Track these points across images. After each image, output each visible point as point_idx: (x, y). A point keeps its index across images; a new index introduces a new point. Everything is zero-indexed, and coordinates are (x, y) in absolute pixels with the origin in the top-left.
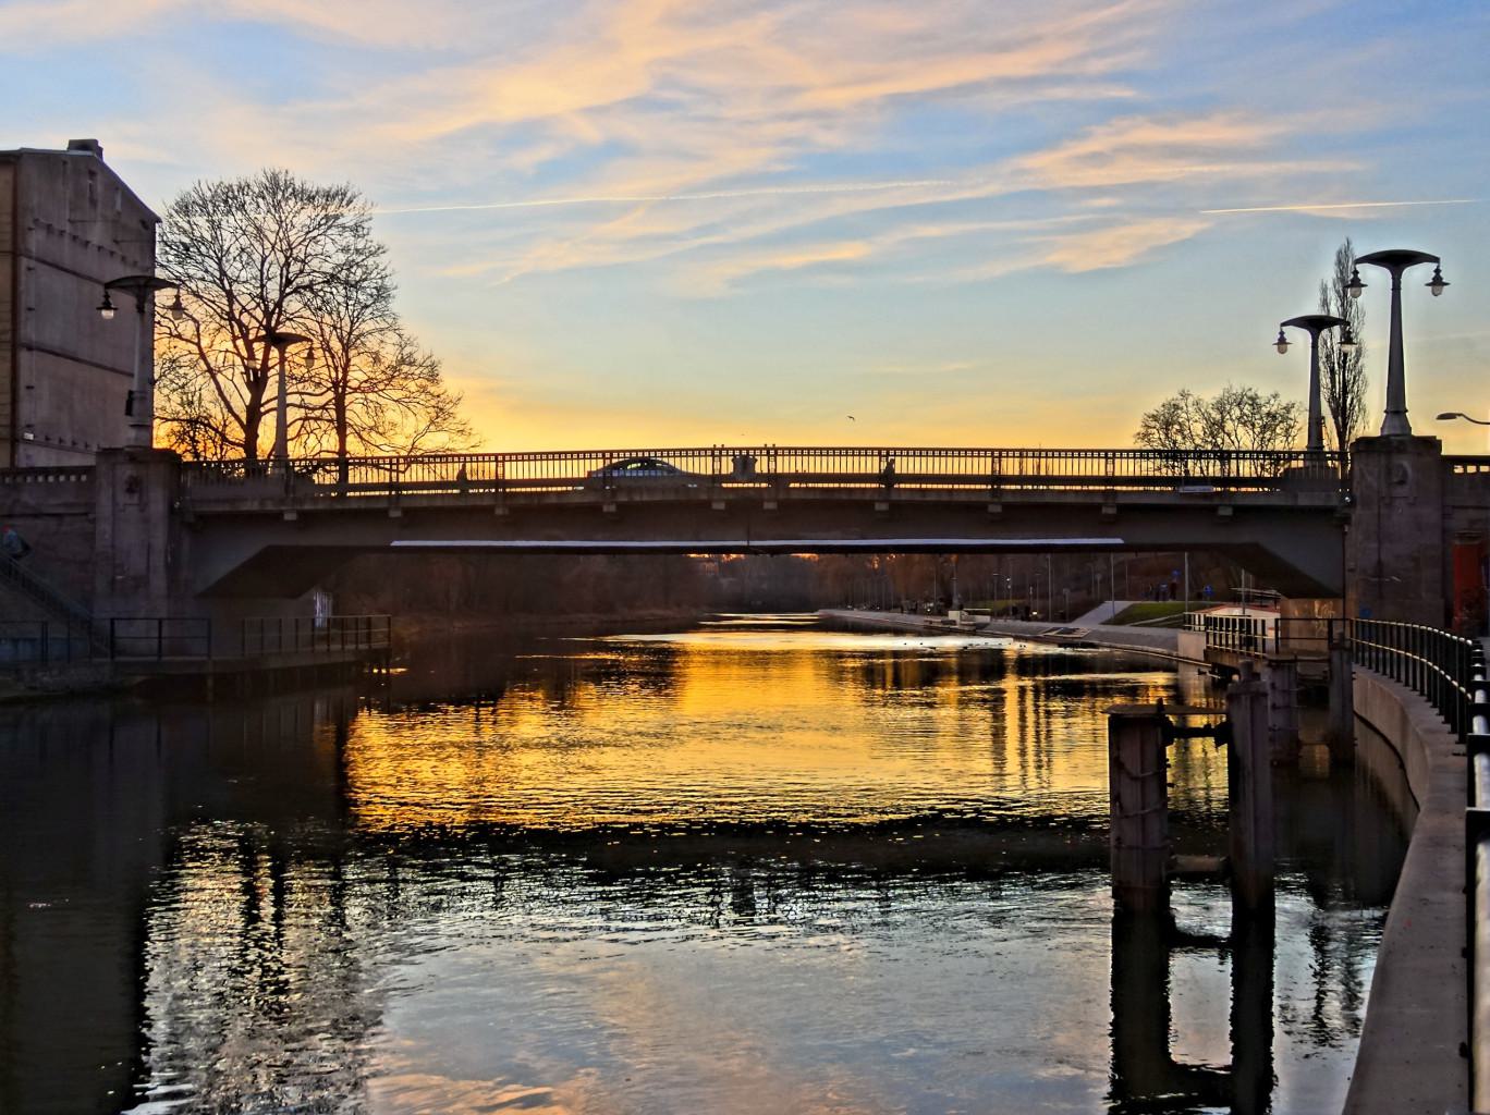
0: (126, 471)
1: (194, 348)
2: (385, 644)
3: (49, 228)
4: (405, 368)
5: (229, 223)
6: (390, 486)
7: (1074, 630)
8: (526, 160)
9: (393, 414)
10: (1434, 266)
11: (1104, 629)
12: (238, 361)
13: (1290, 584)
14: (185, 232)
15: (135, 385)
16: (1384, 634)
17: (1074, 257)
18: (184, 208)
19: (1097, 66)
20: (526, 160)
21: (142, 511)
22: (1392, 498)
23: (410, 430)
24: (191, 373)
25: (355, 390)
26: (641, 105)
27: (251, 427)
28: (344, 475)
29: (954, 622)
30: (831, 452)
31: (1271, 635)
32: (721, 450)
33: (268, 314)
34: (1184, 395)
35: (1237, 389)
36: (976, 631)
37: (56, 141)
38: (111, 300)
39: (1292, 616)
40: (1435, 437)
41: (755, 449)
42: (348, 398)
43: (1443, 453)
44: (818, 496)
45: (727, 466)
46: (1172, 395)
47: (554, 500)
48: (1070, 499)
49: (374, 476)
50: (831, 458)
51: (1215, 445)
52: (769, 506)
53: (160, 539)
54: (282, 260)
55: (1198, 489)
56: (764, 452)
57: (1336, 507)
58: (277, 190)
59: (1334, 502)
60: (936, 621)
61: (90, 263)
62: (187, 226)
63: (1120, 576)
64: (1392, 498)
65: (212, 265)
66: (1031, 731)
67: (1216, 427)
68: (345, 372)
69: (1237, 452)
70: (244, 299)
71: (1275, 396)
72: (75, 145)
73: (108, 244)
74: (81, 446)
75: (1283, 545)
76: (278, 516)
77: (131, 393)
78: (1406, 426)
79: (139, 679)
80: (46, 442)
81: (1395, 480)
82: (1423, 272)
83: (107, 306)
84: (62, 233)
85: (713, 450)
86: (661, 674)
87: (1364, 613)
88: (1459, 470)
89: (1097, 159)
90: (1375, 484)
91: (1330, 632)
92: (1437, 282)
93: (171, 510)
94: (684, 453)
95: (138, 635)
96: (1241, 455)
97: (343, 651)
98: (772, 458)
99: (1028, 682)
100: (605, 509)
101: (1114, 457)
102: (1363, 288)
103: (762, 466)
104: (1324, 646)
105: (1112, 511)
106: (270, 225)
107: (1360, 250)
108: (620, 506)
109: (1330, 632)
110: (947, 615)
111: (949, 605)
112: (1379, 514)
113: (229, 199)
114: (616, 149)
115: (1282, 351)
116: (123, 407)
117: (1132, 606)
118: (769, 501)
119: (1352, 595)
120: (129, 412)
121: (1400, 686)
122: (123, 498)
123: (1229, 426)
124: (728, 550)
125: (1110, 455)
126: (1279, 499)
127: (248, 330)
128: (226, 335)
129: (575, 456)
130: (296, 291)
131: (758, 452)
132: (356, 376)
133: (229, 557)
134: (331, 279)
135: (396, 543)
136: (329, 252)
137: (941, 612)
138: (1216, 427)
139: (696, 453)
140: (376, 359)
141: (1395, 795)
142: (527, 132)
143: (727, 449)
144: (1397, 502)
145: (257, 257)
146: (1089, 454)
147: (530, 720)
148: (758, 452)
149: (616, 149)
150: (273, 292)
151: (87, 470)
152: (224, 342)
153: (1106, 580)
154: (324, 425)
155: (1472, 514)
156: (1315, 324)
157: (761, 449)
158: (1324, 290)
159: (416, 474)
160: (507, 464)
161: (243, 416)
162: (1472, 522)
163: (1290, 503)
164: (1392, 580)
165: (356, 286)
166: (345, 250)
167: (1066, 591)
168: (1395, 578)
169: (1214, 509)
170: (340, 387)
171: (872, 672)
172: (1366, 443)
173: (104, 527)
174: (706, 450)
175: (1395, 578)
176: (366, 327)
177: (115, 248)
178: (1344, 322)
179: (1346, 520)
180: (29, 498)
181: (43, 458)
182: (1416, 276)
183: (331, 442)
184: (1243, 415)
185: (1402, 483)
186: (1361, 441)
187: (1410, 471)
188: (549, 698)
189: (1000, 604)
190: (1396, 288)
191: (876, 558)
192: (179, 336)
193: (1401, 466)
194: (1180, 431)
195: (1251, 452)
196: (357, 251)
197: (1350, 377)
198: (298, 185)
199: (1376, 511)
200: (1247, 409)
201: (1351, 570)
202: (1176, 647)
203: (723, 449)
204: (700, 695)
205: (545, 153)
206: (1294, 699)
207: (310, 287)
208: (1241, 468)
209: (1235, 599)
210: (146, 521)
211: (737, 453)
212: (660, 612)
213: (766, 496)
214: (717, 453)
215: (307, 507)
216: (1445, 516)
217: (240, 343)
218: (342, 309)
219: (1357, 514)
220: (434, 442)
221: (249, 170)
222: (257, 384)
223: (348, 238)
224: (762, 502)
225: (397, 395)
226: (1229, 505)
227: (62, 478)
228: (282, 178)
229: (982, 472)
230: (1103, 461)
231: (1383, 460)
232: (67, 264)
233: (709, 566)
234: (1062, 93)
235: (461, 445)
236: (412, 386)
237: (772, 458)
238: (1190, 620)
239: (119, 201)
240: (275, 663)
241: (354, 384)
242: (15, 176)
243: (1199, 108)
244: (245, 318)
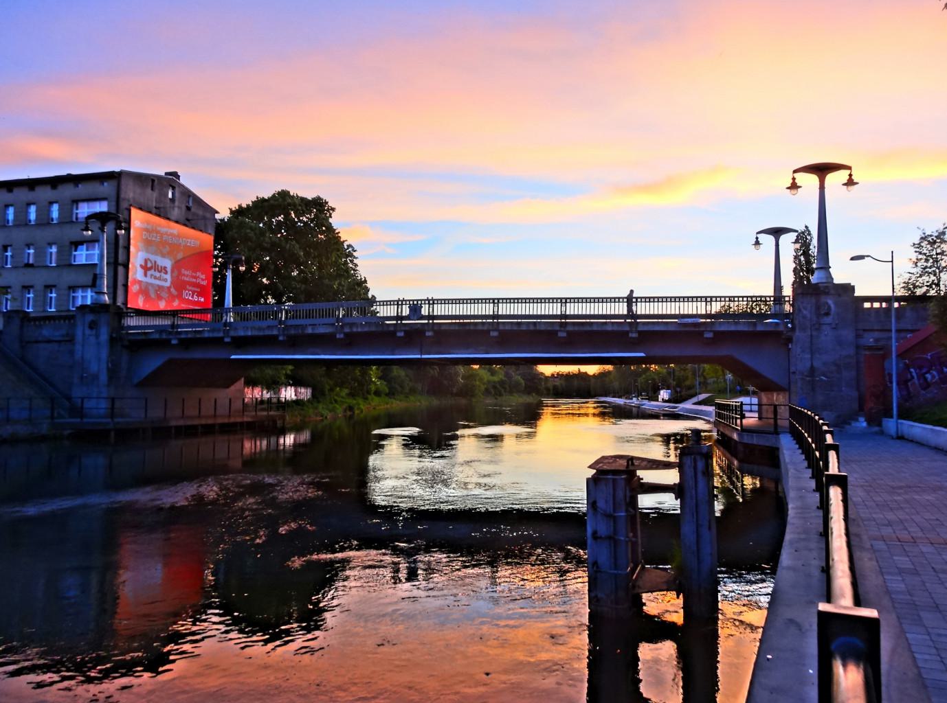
0: (90, 317)
6: (494, 317)
10: (848, 172)
30: (508, 301)
32: (402, 301)
38: (89, 226)
39: (763, 403)
40: (850, 284)
41: (421, 300)
43: (856, 295)
48: (609, 328)
50: (584, 304)
53: (104, 353)
55: (690, 320)
56: (427, 302)
57: (782, 331)
78: (830, 277)
81: (822, 312)
82: (842, 175)
85: (398, 301)
88: (867, 305)
90: (809, 316)
92: (850, 182)
94: (584, 300)
95: (97, 406)
98: (564, 304)
100: (338, 336)
101: (711, 301)
102: (799, 189)
108: (346, 335)
112: (811, 335)
117: (709, 397)
118: (428, 331)
122: (88, 332)
125: (496, 301)
129: (484, 301)
131: (423, 302)
135: (233, 357)
139: (551, 301)
143: (406, 301)
144: (824, 327)
146: (617, 300)
148: (423, 302)
155: (877, 334)
157: (425, 300)
160: (435, 306)
162: (877, 340)
168: (822, 377)
169: (701, 333)
173: (78, 347)
174: (394, 301)
175: (822, 377)
179: (790, 340)
185: (827, 314)
187: (832, 306)
190: (822, 188)
193: (827, 303)
199: (809, 334)
201: (794, 373)
203: (404, 300)
208: (399, 311)
210: (99, 344)
211: (411, 303)
213: (426, 328)
214: (400, 303)
216: (858, 336)
226: (711, 331)
229: (392, 315)
230: (704, 304)
231: (813, 300)
237: (708, 303)
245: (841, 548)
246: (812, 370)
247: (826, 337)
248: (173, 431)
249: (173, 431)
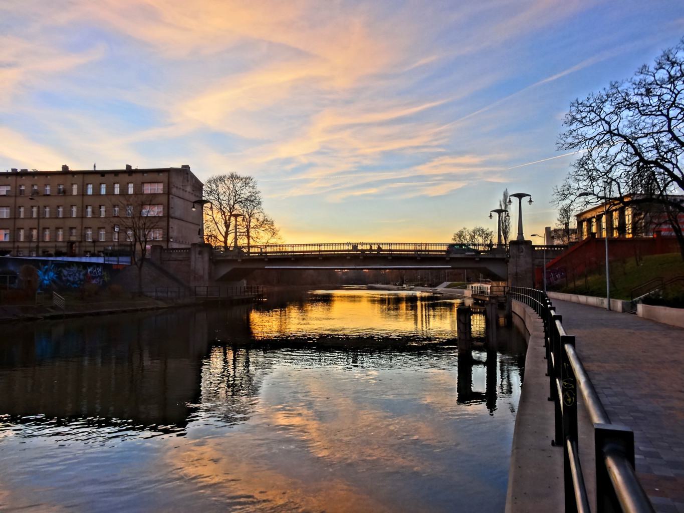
0: (198, 249)
1: (212, 217)
2: (261, 293)
3: (177, 187)
4: (265, 222)
5: (220, 186)
7: (436, 290)
8: (288, 167)
9: (262, 234)
11: (444, 289)
12: (223, 220)
13: (491, 277)
14: (209, 187)
15: (200, 227)
16: (518, 290)
17: (431, 192)
18: (209, 182)
19: (436, 143)
20: (288, 167)
21: (202, 259)
22: (520, 256)
23: (266, 238)
24: (211, 224)
25: (253, 228)
26: (318, 153)
27: (226, 237)
28: (249, 250)
29: (405, 288)
31: (489, 291)
33: (230, 209)
34: (464, 229)
35: (478, 227)
36: (411, 289)
37: (178, 165)
42: (250, 230)
44: (374, 255)
45: (351, 248)
46: (461, 229)
47: (307, 256)
48: (438, 256)
49: (256, 250)
51: (472, 241)
52: (361, 258)
53: (207, 267)
54: (234, 195)
58: (233, 177)
59: (505, 257)
60: (400, 287)
61: (187, 196)
62: (210, 186)
63: (448, 276)
64: (520, 256)
65: (216, 196)
66: (424, 317)
67: (472, 237)
68: (249, 223)
69: (478, 244)
70: (224, 205)
71: (488, 229)
72: (183, 166)
73: (191, 192)
74: (184, 242)
75: (495, 269)
76: (237, 260)
77: (200, 229)
79: (201, 302)
80: (176, 242)
82: (528, 198)
83: (194, 208)
84: (180, 189)
86: (327, 300)
87: (512, 285)
89: (436, 167)
91: (504, 290)
92: (530, 201)
93: (210, 259)
95: (202, 290)
96: (479, 245)
97: (249, 295)
99: (423, 303)
103: (359, 248)
104: (503, 293)
105: (448, 259)
106: (231, 186)
107: (511, 192)
109: (504, 290)
110: (605, 238)
111: (403, 283)
113: (222, 179)
114: (311, 165)
115: (491, 218)
116: (198, 233)
119: (509, 280)
120: (199, 234)
121: (525, 304)
122: (197, 256)
123: (476, 237)
124: (345, 269)
126: (490, 256)
127: (225, 213)
128: (220, 214)
130: (238, 203)
132: (252, 225)
133: (224, 270)
134: (246, 200)
135: (266, 267)
136: (246, 193)
137: (401, 285)
138: (472, 237)
140: (258, 220)
141: (522, 330)
142: (288, 161)
145: (228, 194)
147: (294, 313)
149: (311, 165)
150: (232, 202)
151: (189, 249)
152: (219, 215)
153: (445, 276)
154: (244, 237)
156: (499, 212)
158: (500, 202)
159: (269, 249)
161: (224, 234)
163: (493, 257)
165: (253, 201)
166: (250, 192)
167: (434, 280)
170: (248, 228)
171: (382, 301)
172: (512, 242)
173: (193, 263)
176: (254, 212)
177: (193, 192)
178: (506, 211)
179: (508, 261)
180: (173, 256)
181: (175, 246)
182: (525, 200)
183: (246, 241)
184: (480, 234)
185: (522, 252)
186: (511, 241)
187: (524, 249)
188: (299, 309)
189: (417, 283)
190: (520, 203)
191: (383, 271)
192: (208, 214)
194: (463, 238)
195: (482, 244)
196: (253, 193)
197: (507, 224)
198: (238, 176)
200: (481, 232)
201: (509, 274)
202: (463, 294)
204: (338, 307)
205: (293, 166)
206: (497, 306)
207: (241, 202)
209: (479, 282)
212: (327, 285)
215: (244, 258)
216: (533, 260)
217: (223, 216)
218: (249, 207)
219: (511, 260)
220: (272, 241)
221: (226, 171)
222: (227, 226)
223: (251, 189)
224: (359, 257)
225: (263, 229)
227: (174, 251)
228: (234, 174)
232: (181, 196)
233: (340, 273)
234: (426, 150)
235: (279, 243)
236: (267, 227)
238: (466, 287)
239: (194, 180)
240: (236, 298)
241: (252, 226)
242: (169, 175)
243: (461, 153)
244: (224, 210)
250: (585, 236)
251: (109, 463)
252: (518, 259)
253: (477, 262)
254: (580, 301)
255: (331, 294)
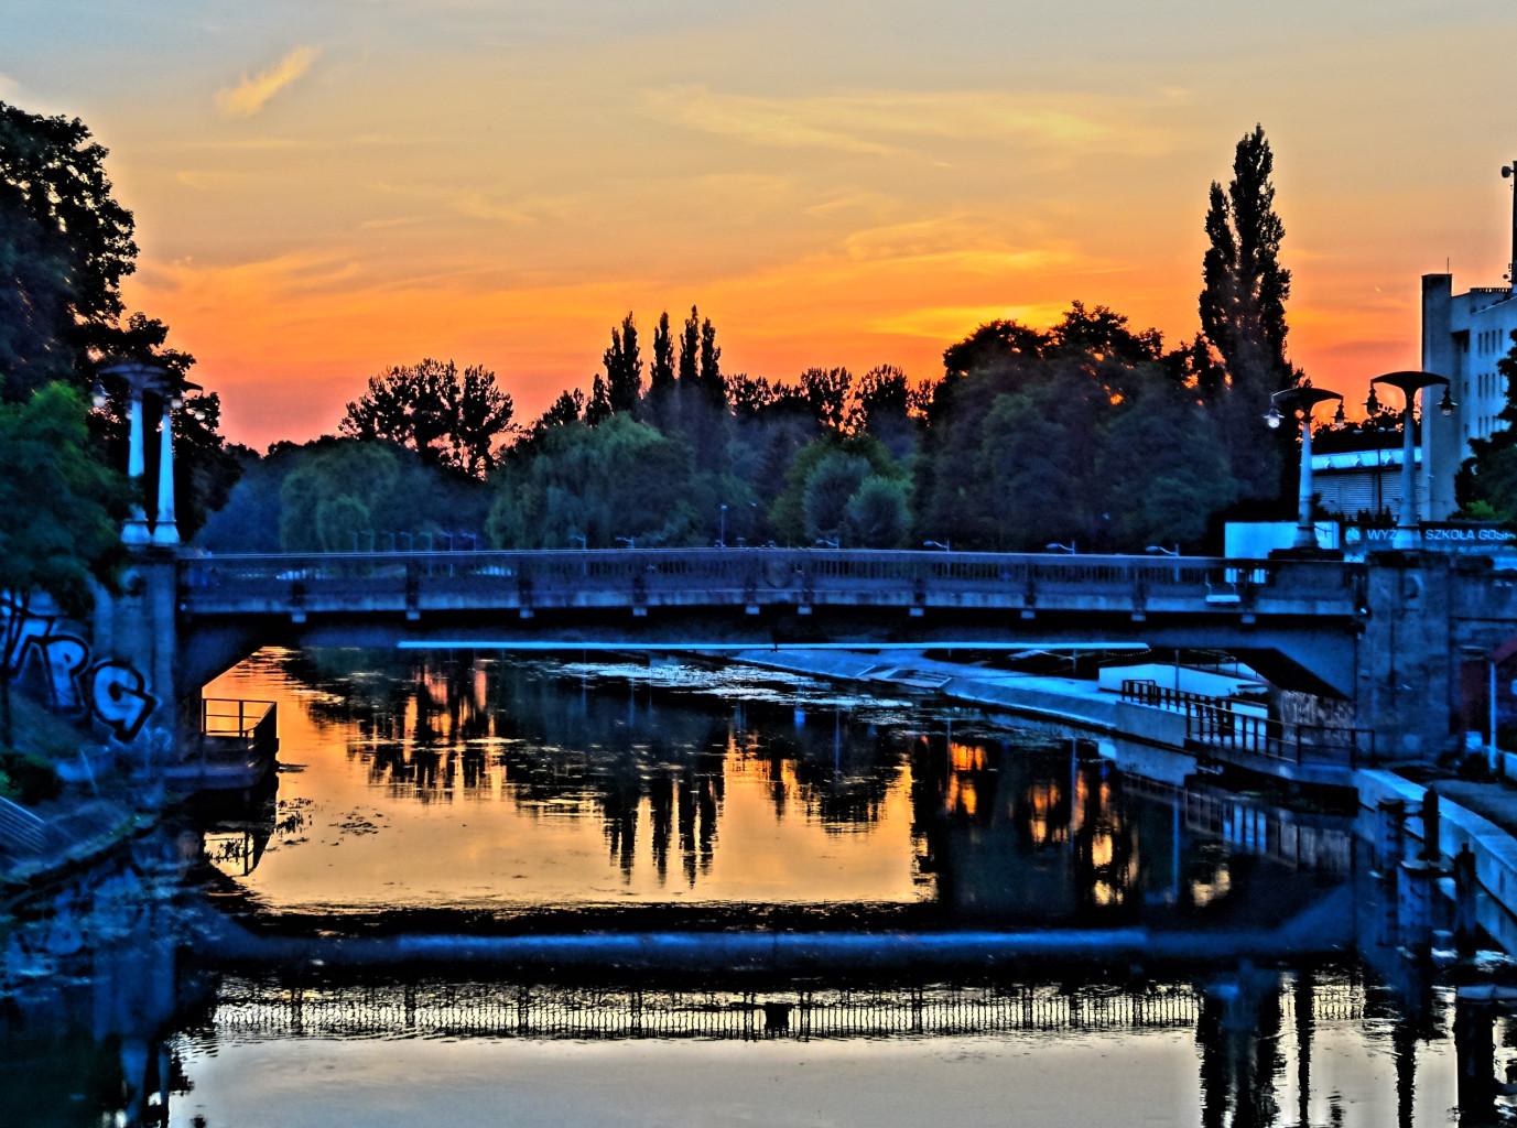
22: (1405, 610)
64: (1405, 610)
108: (651, 610)
118: (804, 606)
144: (1409, 614)
155: (1475, 625)
164: (1404, 689)
179: (1362, 629)
185: (1414, 596)
193: (1412, 581)
216: (1452, 627)
219: (1373, 624)
231: (1396, 574)
245: (1442, 1079)
246: (1393, 675)
247: (1411, 629)
248: (492, 726)
249: (492, 726)
250: (1455, 535)
251: (288, 73)
252: (1397, 622)
253: (1248, 629)
254: (1115, 745)
255: (626, 677)
